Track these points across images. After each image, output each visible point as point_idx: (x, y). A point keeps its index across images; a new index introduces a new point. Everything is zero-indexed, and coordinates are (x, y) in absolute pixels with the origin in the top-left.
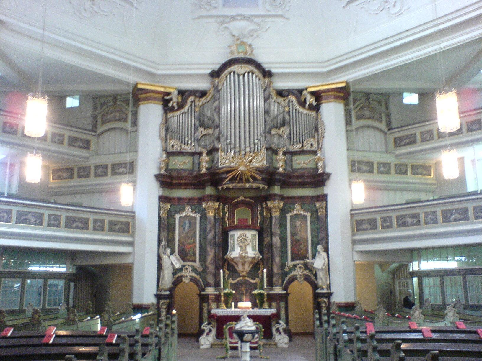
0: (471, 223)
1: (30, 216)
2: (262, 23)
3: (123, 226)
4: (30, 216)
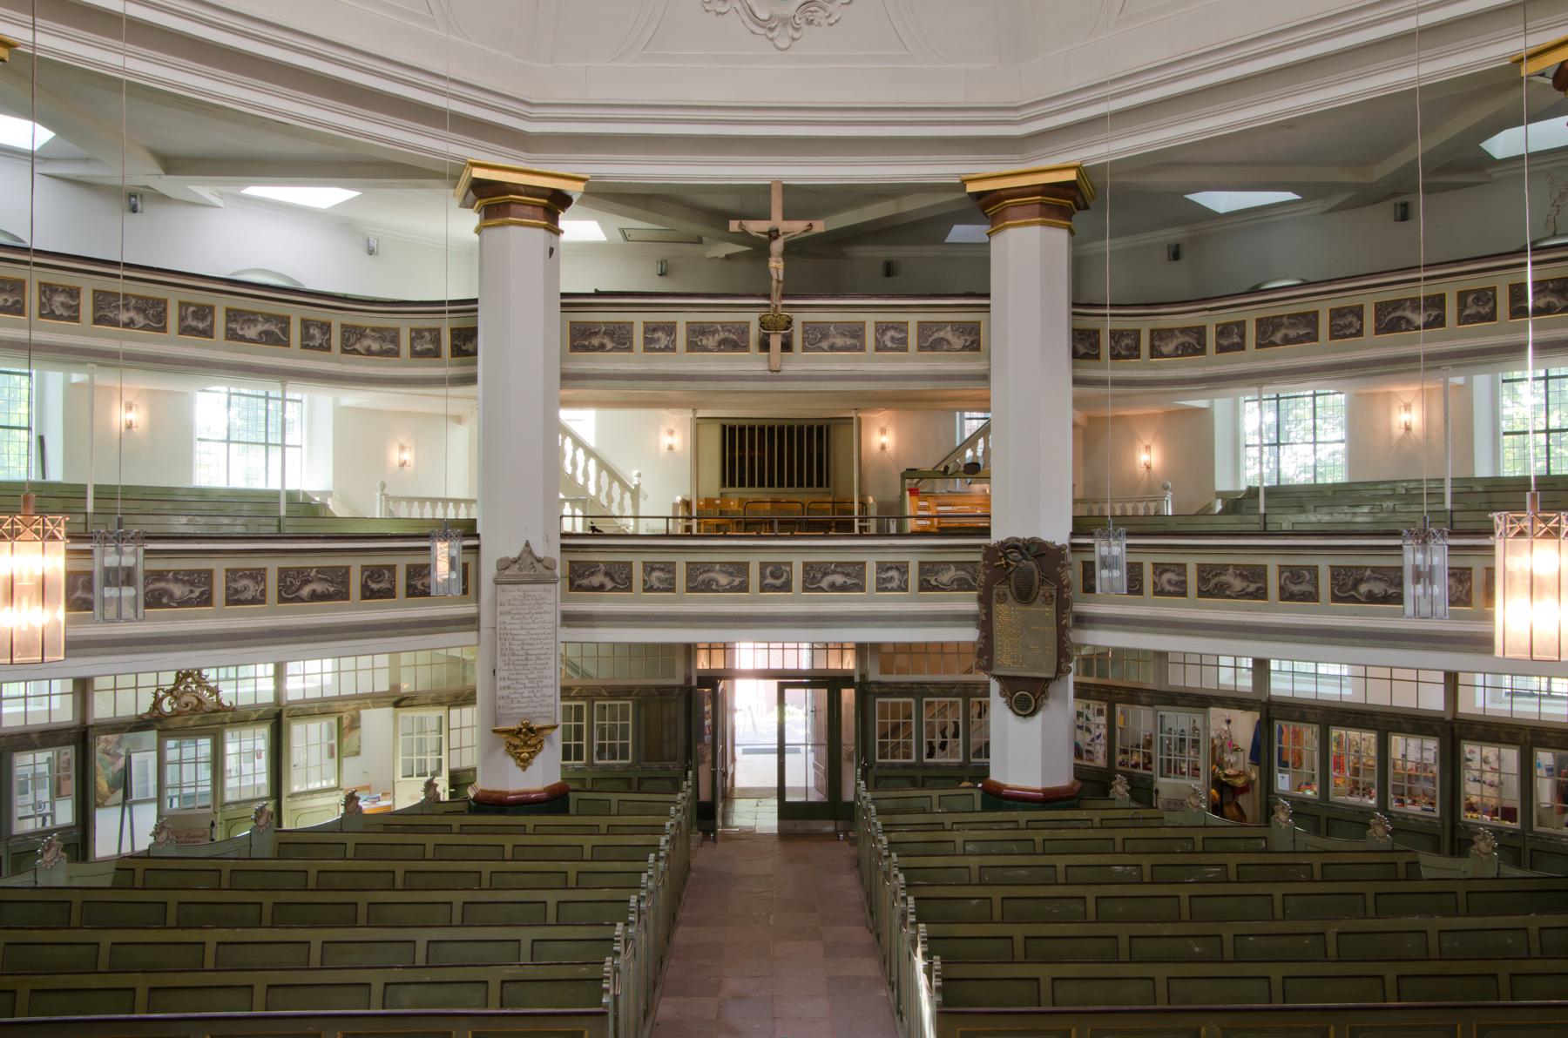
0: (403, 365)
1: (947, 334)
3: (962, 574)
4: (1228, 578)
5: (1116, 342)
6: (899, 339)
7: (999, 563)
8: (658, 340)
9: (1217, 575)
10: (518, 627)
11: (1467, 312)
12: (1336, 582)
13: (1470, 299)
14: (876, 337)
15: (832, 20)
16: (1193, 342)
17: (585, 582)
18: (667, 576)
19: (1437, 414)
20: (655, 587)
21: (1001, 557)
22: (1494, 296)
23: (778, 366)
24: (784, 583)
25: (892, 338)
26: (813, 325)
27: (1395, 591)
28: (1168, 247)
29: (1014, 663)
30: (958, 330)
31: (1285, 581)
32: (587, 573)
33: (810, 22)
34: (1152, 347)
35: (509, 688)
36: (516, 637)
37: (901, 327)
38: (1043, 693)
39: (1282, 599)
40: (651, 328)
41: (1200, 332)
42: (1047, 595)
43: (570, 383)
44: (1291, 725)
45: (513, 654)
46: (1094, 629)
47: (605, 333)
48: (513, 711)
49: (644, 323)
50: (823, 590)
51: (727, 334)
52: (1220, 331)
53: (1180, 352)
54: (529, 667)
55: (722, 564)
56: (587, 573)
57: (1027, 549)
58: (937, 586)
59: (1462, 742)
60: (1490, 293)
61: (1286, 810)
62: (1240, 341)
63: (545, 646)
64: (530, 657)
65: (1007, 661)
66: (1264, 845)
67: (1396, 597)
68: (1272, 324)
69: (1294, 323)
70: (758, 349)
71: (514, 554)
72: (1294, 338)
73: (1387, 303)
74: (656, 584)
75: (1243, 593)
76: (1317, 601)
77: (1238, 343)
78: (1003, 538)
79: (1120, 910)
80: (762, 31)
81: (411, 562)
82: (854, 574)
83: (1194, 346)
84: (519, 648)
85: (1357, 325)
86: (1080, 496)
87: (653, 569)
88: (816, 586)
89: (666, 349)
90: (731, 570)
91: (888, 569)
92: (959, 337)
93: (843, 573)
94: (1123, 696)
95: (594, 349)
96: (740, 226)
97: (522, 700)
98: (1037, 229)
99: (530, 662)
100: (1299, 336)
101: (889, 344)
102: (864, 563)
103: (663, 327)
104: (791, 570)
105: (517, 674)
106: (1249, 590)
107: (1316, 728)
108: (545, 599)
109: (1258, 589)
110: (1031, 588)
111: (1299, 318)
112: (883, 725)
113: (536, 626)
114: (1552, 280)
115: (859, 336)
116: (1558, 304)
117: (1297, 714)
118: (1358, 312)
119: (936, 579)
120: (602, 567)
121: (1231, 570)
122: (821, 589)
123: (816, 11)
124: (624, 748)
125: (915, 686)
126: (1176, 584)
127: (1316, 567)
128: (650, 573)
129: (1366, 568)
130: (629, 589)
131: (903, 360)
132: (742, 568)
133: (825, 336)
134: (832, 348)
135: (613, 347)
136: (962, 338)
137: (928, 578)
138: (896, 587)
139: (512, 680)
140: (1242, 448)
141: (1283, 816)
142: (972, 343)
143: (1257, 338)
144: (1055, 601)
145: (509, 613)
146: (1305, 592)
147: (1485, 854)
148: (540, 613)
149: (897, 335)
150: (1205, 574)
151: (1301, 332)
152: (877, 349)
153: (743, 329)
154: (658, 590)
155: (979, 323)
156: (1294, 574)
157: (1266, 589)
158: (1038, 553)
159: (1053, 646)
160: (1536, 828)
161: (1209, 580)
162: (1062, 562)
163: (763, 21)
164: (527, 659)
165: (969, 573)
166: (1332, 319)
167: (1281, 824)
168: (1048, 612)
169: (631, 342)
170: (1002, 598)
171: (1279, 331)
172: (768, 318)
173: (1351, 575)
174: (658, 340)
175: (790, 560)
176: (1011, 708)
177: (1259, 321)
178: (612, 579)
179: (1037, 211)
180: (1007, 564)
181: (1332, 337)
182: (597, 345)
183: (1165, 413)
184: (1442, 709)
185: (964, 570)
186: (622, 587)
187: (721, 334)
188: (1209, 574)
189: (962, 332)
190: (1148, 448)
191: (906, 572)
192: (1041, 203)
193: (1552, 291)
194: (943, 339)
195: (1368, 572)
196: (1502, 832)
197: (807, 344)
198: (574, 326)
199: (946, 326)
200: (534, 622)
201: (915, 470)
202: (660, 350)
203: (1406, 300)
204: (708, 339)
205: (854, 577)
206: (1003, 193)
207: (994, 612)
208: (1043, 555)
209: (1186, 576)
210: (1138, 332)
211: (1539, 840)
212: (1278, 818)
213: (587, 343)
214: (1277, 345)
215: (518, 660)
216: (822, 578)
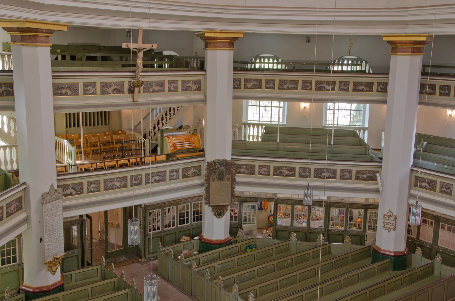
1: (190, 84)
3: (195, 170)
4: (284, 170)
6: (176, 87)
7: (213, 168)
9: (280, 169)
10: (50, 219)
11: (341, 88)
12: (316, 172)
13: (342, 84)
14: (168, 86)
16: (258, 84)
18: (97, 186)
20: (92, 191)
22: (349, 84)
31: (301, 172)
34: (245, 85)
35: (49, 245)
36: (50, 224)
40: (86, 85)
41: (260, 81)
42: (228, 178)
44: (283, 205)
45: (50, 231)
47: (67, 87)
48: (51, 254)
49: (83, 83)
51: (116, 86)
52: (267, 82)
53: (253, 87)
54: (55, 234)
55: (117, 178)
57: (222, 163)
58: (188, 176)
60: (348, 83)
61: (295, 236)
62: (273, 86)
63: (60, 224)
64: (55, 230)
66: (288, 246)
67: (332, 177)
68: (284, 82)
69: (291, 83)
70: (128, 93)
71: (47, 190)
72: (291, 88)
74: (93, 189)
75: (288, 175)
77: (272, 87)
79: (285, 282)
81: (6, 203)
83: (258, 86)
84: (51, 228)
85: (310, 86)
86: (232, 139)
87: (91, 184)
89: (93, 93)
90: (120, 180)
91: (173, 172)
92: (194, 86)
95: (63, 95)
97: (53, 248)
98: (227, 51)
99: (55, 232)
100: (292, 87)
103: (91, 84)
105: (51, 238)
106: (290, 174)
107: (291, 206)
108: (59, 206)
109: (292, 174)
110: (223, 176)
111: (293, 82)
113: (56, 217)
114: (364, 82)
115: (163, 86)
116: (365, 89)
117: (285, 202)
118: (310, 82)
119: (187, 174)
121: (284, 168)
126: (266, 172)
128: (90, 186)
132: (125, 179)
135: (71, 94)
136: (196, 86)
137: (185, 173)
138: (175, 178)
139: (50, 241)
141: (294, 237)
143: (279, 86)
145: (48, 215)
146: (307, 175)
148: (57, 212)
150: (276, 169)
151: (293, 86)
152: (169, 91)
153: (122, 84)
154: (94, 192)
155: (200, 80)
156: (304, 170)
157: (295, 174)
160: (348, 229)
161: (277, 171)
162: (233, 167)
164: (54, 232)
165: (197, 169)
166: (302, 84)
167: (293, 239)
168: (228, 183)
170: (213, 180)
171: (286, 85)
172: (135, 82)
175: (141, 174)
176: (216, 215)
177: (280, 80)
178: (75, 190)
180: (216, 169)
181: (302, 89)
182: (64, 93)
185: (196, 169)
186: (79, 192)
187: (114, 87)
188: (277, 169)
189: (195, 83)
191: (178, 172)
192: (228, 42)
193: (364, 85)
196: (340, 231)
197: (145, 90)
199: (191, 82)
200: (56, 216)
202: (90, 94)
203: (325, 81)
204: (109, 89)
205: (162, 176)
209: (270, 169)
211: (349, 232)
212: (292, 238)
213: (60, 92)
215: (51, 233)
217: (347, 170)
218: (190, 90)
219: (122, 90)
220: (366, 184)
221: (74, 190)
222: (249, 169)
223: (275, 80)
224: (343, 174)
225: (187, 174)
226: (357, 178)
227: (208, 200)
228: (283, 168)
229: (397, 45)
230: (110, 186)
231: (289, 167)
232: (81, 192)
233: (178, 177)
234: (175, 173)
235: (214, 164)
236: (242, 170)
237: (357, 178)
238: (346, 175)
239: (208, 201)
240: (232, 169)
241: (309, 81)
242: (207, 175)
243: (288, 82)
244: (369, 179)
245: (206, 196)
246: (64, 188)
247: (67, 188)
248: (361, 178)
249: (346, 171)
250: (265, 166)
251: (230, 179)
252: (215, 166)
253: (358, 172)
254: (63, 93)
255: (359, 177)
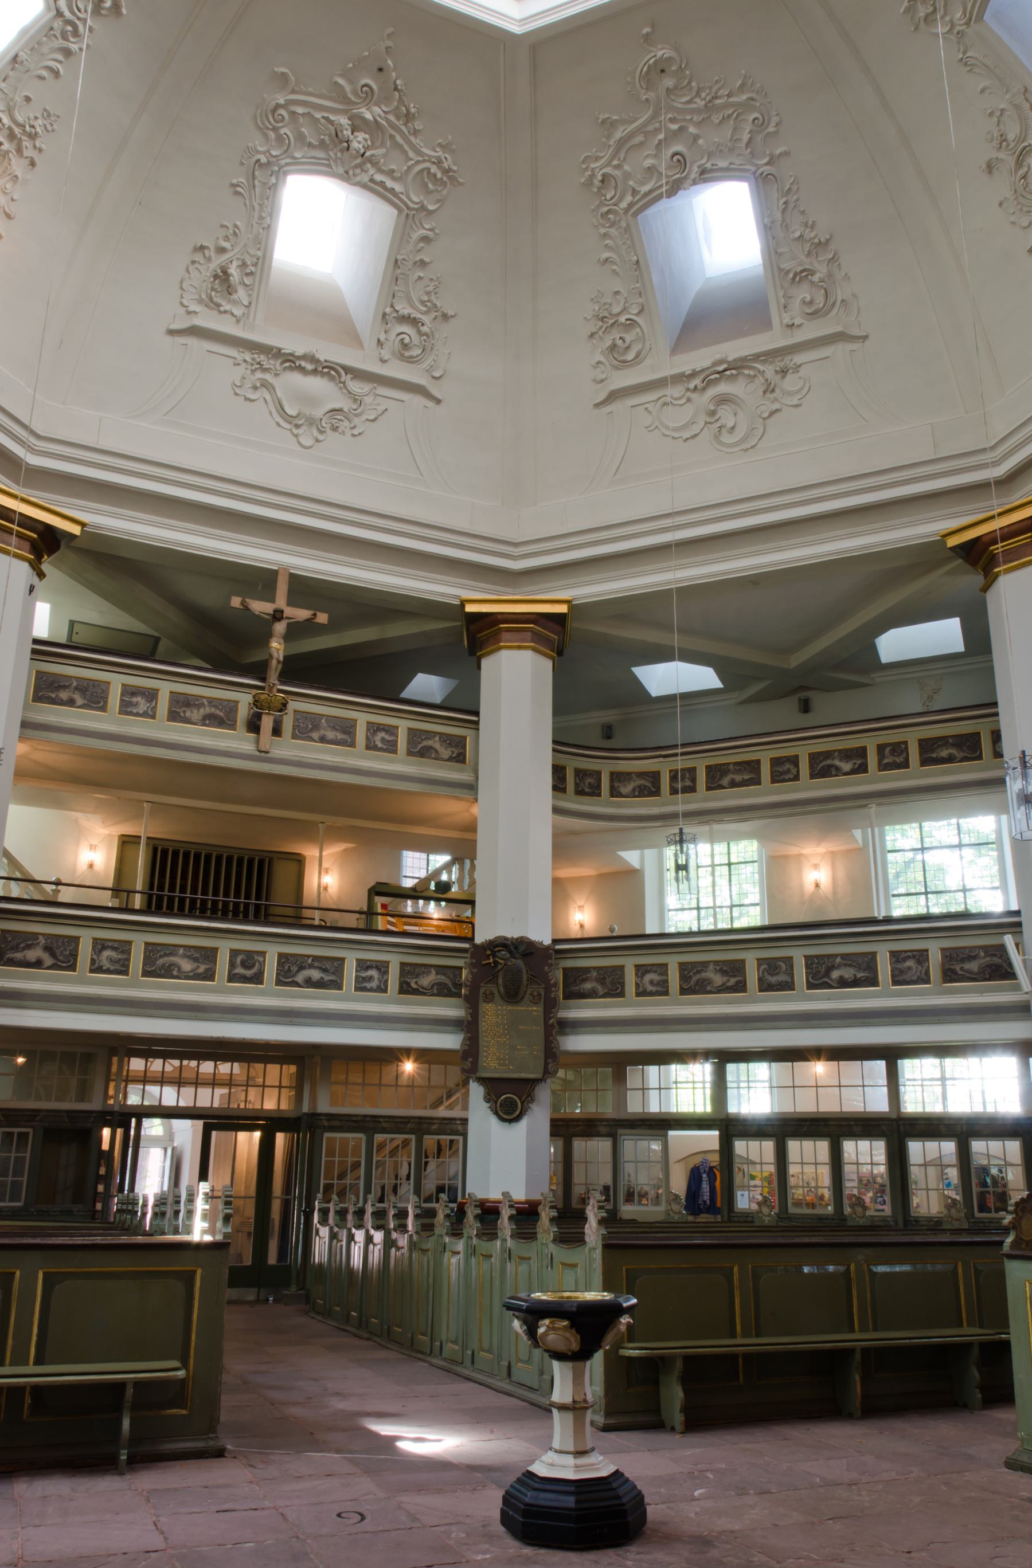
2: (368, 400)
3: (442, 978)
4: (710, 974)
5: (581, 780)
8: (137, 704)
9: (698, 972)
11: (886, 761)
13: (888, 750)
14: (367, 736)
15: (356, 432)
17: (18, 955)
18: (121, 956)
19: (841, 874)
20: (104, 968)
21: (489, 955)
22: (906, 748)
23: (268, 747)
24: (255, 974)
25: (383, 740)
26: (305, 715)
27: (863, 975)
28: (603, 726)
29: (500, 1065)
30: (445, 741)
31: (763, 972)
32: (22, 945)
33: (335, 429)
37: (392, 730)
38: (529, 1095)
39: (761, 990)
41: (655, 776)
42: (535, 993)
43: (30, 732)
46: (576, 1034)
47: (76, 688)
50: (298, 985)
51: (213, 709)
53: (637, 793)
56: (22, 945)
57: (516, 948)
58: (417, 990)
59: (907, 1139)
60: (903, 746)
61: (768, 1203)
62: (691, 784)
65: (491, 1064)
67: (865, 980)
70: (246, 729)
73: (818, 753)
74: (106, 965)
76: (794, 989)
77: (689, 786)
78: (491, 936)
80: (288, 426)
82: (332, 970)
87: (104, 948)
88: (290, 980)
89: (145, 715)
90: (197, 955)
91: (368, 968)
93: (320, 968)
94: (581, 1128)
95: (62, 703)
96: (243, 603)
101: (380, 745)
102: (343, 960)
104: (264, 961)
106: (729, 984)
109: (737, 983)
112: (330, 1165)
115: (351, 732)
116: (958, 755)
118: (794, 760)
120: (42, 940)
121: (711, 967)
122: (296, 984)
123: (341, 420)
124: (16, 1186)
125: (368, 1119)
126: (658, 984)
127: (791, 958)
128: (100, 951)
129: (836, 956)
130: (72, 967)
131: (393, 762)
133: (316, 727)
134: (323, 740)
135: (84, 704)
136: (450, 749)
137: (408, 980)
140: (666, 911)
142: (459, 755)
143: (707, 782)
144: (542, 1000)
147: (957, 1220)
149: (387, 737)
151: (746, 777)
153: (232, 707)
154: (108, 971)
158: (526, 952)
159: (539, 1050)
161: (690, 977)
163: (291, 417)
165: (449, 977)
166: (772, 766)
168: (535, 1011)
169: (106, 702)
170: (489, 998)
171: (726, 776)
172: (263, 697)
173: (824, 963)
174: (137, 704)
176: (496, 1113)
178: (53, 955)
179: (529, 638)
180: (496, 963)
181: (773, 781)
183: (602, 876)
184: (887, 1110)
185: (445, 974)
186: (64, 965)
187: (207, 708)
188: (690, 972)
190: (581, 907)
191: (386, 972)
194: (431, 747)
195: (838, 960)
197: (297, 732)
198: (40, 675)
199: (435, 736)
201: (386, 884)
202: (137, 715)
203: (835, 751)
204: (192, 712)
206: (499, 617)
207: (481, 1012)
208: (531, 954)
210: (599, 774)
213: (53, 696)
214: (725, 788)
216: (298, 971)
217: (909, 954)
218: (433, 756)
219: (229, 720)
220: (981, 991)
221: (48, 954)
222: (608, 980)
223: (694, 769)
224: (899, 966)
225: (416, 983)
226: (950, 976)
227: (470, 1059)
228: (706, 967)
229: (991, 548)
230: (163, 965)
231: (724, 962)
232: (70, 966)
233: (383, 987)
234: (373, 973)
235: (491, 950)
236: (588, 986)
237: (950, 976)
238: (910, 968)
239: (471, 1062)
240: (546, 968)
241: (790, 756)
242: (469, 984)
243: (731, 767)
244: (990, 974)
245: (467, 1048)
246: (21, 943)
247: (30, 942)
248: (962, 973)
249: (909, 956)
250: (653, 965)
251: (540, 999)
252: (494, 955)
253: (947, 956)
254: (62, 700)
255: (953, 971)
